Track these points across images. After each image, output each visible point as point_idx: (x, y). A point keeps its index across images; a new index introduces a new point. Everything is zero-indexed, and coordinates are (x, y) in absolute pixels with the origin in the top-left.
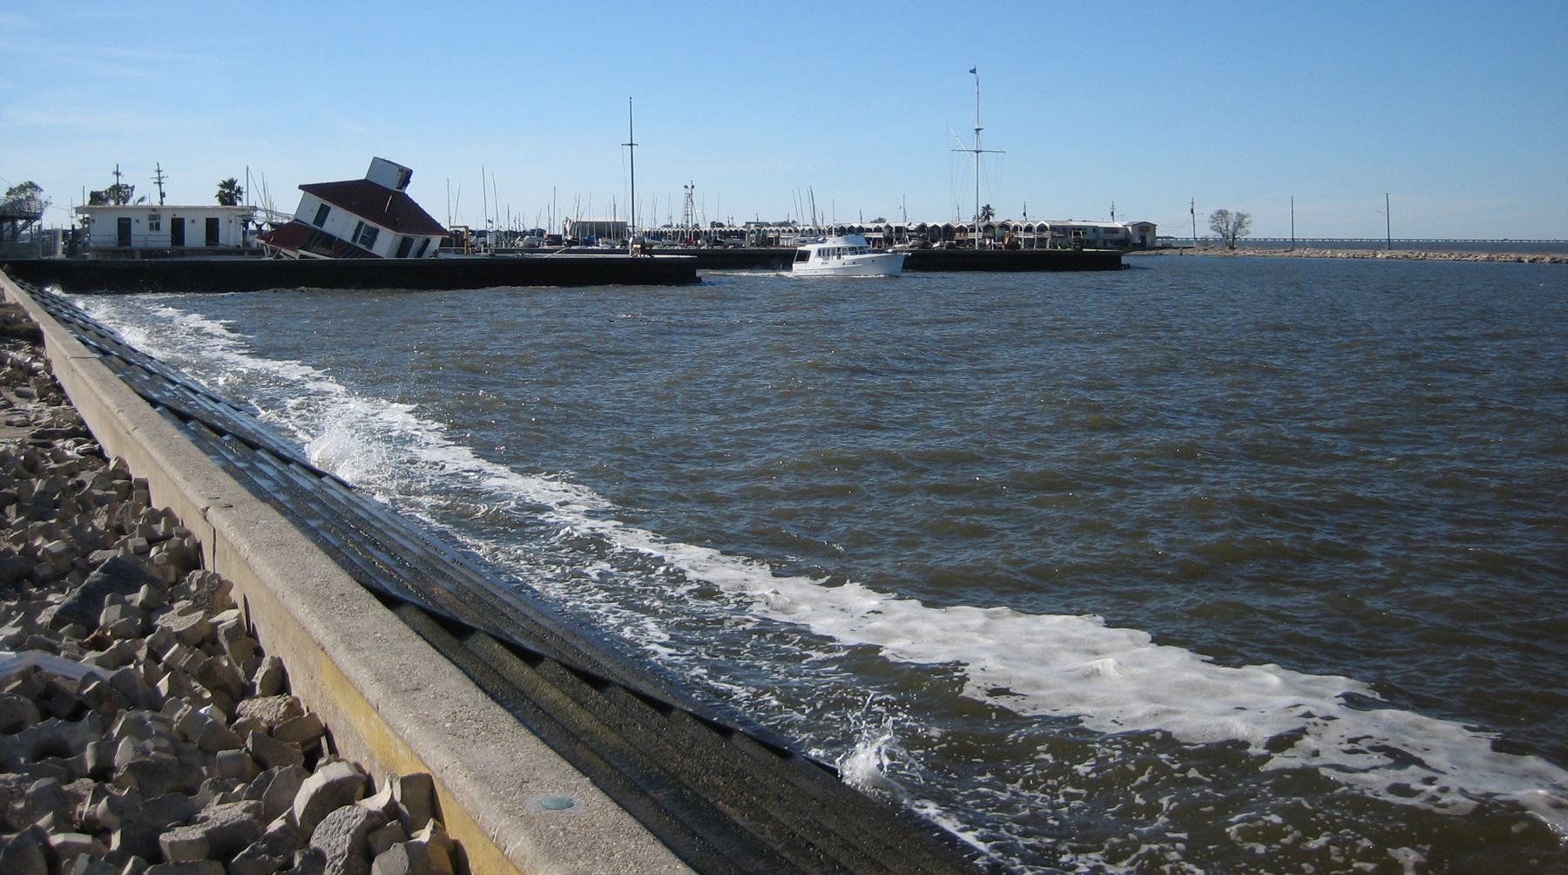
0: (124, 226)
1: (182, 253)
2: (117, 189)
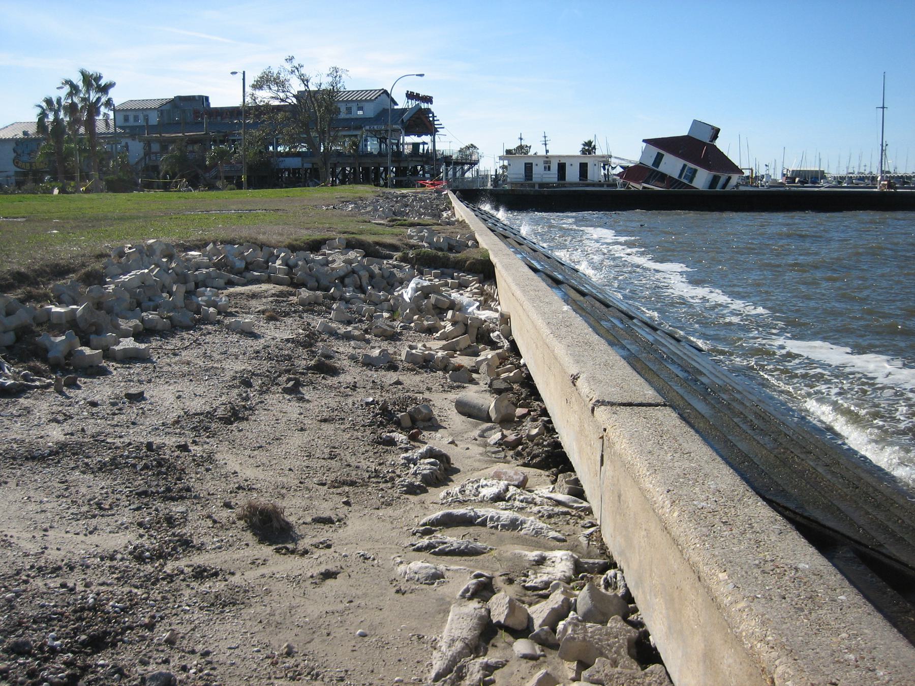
0: (529, 167)
1: (563, 185)
2: (521, 147)
